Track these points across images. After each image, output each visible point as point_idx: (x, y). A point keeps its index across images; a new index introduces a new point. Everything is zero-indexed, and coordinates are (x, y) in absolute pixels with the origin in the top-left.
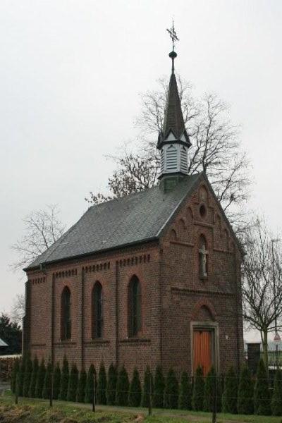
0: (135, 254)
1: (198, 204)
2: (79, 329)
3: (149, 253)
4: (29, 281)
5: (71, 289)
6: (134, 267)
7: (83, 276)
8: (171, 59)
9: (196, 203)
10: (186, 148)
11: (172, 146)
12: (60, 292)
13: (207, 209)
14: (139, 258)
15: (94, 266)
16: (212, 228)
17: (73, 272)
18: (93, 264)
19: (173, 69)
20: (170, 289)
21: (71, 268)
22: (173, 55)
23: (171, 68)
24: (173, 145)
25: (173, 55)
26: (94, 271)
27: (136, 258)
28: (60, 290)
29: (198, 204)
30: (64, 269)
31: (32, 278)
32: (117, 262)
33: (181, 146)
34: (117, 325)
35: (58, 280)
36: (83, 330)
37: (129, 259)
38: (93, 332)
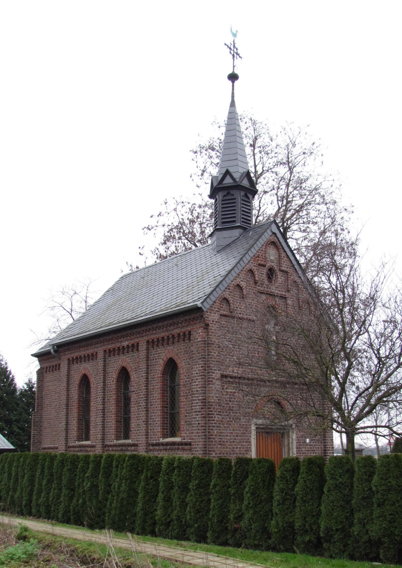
0: (121, 342)
1: (264, 266)
2: (100, 428)
3: (189, 328)
4: (41, 368)
5: (90, 377)
6: (122, 357)
7: (105, 361)
8: (230, 83)
9: (260, 265)
10: (250, 196)
11: (228, 193)
12: (77, 382)
13: (279, 274)
14: (176, 335)
15: (119, 348)
16: (285, 298)
17: (93, 357)
18: (118, 345)
19: (233, 96)
20: (219, 376)
21: (90, 351)
22: (233, 77)
23: (231, 95)
24: (232, 192)
25: (233, 77)
26: (119, 354)
27: (173, 336)
28: (76, 379)
29: (264, 266)
30: (82, 353)
31: (43, 366)
32: (148, 342)
33: (243, 193)
34: (147, 422)
35: (75, 366)
36: (104, 429)
37: (163, 338)
38: (118, 431)
